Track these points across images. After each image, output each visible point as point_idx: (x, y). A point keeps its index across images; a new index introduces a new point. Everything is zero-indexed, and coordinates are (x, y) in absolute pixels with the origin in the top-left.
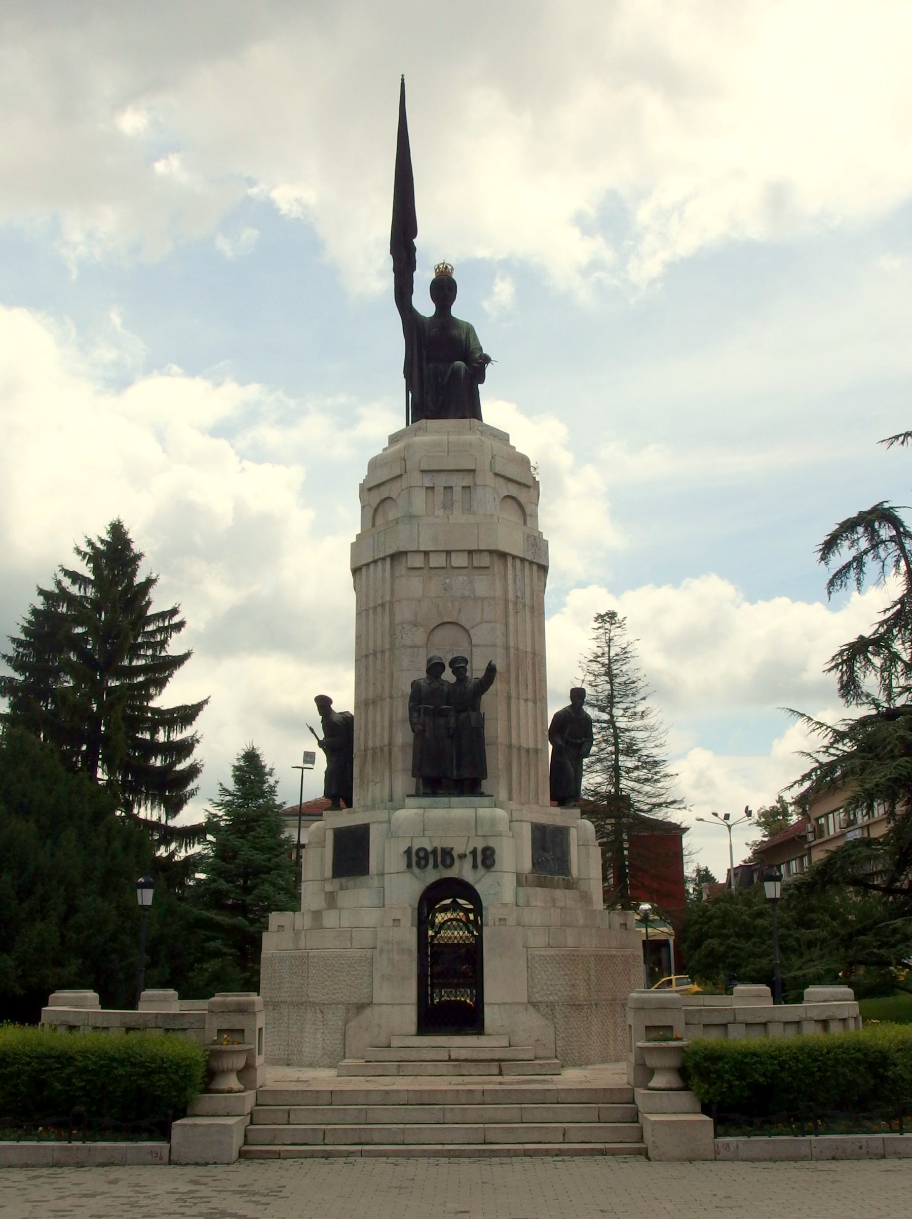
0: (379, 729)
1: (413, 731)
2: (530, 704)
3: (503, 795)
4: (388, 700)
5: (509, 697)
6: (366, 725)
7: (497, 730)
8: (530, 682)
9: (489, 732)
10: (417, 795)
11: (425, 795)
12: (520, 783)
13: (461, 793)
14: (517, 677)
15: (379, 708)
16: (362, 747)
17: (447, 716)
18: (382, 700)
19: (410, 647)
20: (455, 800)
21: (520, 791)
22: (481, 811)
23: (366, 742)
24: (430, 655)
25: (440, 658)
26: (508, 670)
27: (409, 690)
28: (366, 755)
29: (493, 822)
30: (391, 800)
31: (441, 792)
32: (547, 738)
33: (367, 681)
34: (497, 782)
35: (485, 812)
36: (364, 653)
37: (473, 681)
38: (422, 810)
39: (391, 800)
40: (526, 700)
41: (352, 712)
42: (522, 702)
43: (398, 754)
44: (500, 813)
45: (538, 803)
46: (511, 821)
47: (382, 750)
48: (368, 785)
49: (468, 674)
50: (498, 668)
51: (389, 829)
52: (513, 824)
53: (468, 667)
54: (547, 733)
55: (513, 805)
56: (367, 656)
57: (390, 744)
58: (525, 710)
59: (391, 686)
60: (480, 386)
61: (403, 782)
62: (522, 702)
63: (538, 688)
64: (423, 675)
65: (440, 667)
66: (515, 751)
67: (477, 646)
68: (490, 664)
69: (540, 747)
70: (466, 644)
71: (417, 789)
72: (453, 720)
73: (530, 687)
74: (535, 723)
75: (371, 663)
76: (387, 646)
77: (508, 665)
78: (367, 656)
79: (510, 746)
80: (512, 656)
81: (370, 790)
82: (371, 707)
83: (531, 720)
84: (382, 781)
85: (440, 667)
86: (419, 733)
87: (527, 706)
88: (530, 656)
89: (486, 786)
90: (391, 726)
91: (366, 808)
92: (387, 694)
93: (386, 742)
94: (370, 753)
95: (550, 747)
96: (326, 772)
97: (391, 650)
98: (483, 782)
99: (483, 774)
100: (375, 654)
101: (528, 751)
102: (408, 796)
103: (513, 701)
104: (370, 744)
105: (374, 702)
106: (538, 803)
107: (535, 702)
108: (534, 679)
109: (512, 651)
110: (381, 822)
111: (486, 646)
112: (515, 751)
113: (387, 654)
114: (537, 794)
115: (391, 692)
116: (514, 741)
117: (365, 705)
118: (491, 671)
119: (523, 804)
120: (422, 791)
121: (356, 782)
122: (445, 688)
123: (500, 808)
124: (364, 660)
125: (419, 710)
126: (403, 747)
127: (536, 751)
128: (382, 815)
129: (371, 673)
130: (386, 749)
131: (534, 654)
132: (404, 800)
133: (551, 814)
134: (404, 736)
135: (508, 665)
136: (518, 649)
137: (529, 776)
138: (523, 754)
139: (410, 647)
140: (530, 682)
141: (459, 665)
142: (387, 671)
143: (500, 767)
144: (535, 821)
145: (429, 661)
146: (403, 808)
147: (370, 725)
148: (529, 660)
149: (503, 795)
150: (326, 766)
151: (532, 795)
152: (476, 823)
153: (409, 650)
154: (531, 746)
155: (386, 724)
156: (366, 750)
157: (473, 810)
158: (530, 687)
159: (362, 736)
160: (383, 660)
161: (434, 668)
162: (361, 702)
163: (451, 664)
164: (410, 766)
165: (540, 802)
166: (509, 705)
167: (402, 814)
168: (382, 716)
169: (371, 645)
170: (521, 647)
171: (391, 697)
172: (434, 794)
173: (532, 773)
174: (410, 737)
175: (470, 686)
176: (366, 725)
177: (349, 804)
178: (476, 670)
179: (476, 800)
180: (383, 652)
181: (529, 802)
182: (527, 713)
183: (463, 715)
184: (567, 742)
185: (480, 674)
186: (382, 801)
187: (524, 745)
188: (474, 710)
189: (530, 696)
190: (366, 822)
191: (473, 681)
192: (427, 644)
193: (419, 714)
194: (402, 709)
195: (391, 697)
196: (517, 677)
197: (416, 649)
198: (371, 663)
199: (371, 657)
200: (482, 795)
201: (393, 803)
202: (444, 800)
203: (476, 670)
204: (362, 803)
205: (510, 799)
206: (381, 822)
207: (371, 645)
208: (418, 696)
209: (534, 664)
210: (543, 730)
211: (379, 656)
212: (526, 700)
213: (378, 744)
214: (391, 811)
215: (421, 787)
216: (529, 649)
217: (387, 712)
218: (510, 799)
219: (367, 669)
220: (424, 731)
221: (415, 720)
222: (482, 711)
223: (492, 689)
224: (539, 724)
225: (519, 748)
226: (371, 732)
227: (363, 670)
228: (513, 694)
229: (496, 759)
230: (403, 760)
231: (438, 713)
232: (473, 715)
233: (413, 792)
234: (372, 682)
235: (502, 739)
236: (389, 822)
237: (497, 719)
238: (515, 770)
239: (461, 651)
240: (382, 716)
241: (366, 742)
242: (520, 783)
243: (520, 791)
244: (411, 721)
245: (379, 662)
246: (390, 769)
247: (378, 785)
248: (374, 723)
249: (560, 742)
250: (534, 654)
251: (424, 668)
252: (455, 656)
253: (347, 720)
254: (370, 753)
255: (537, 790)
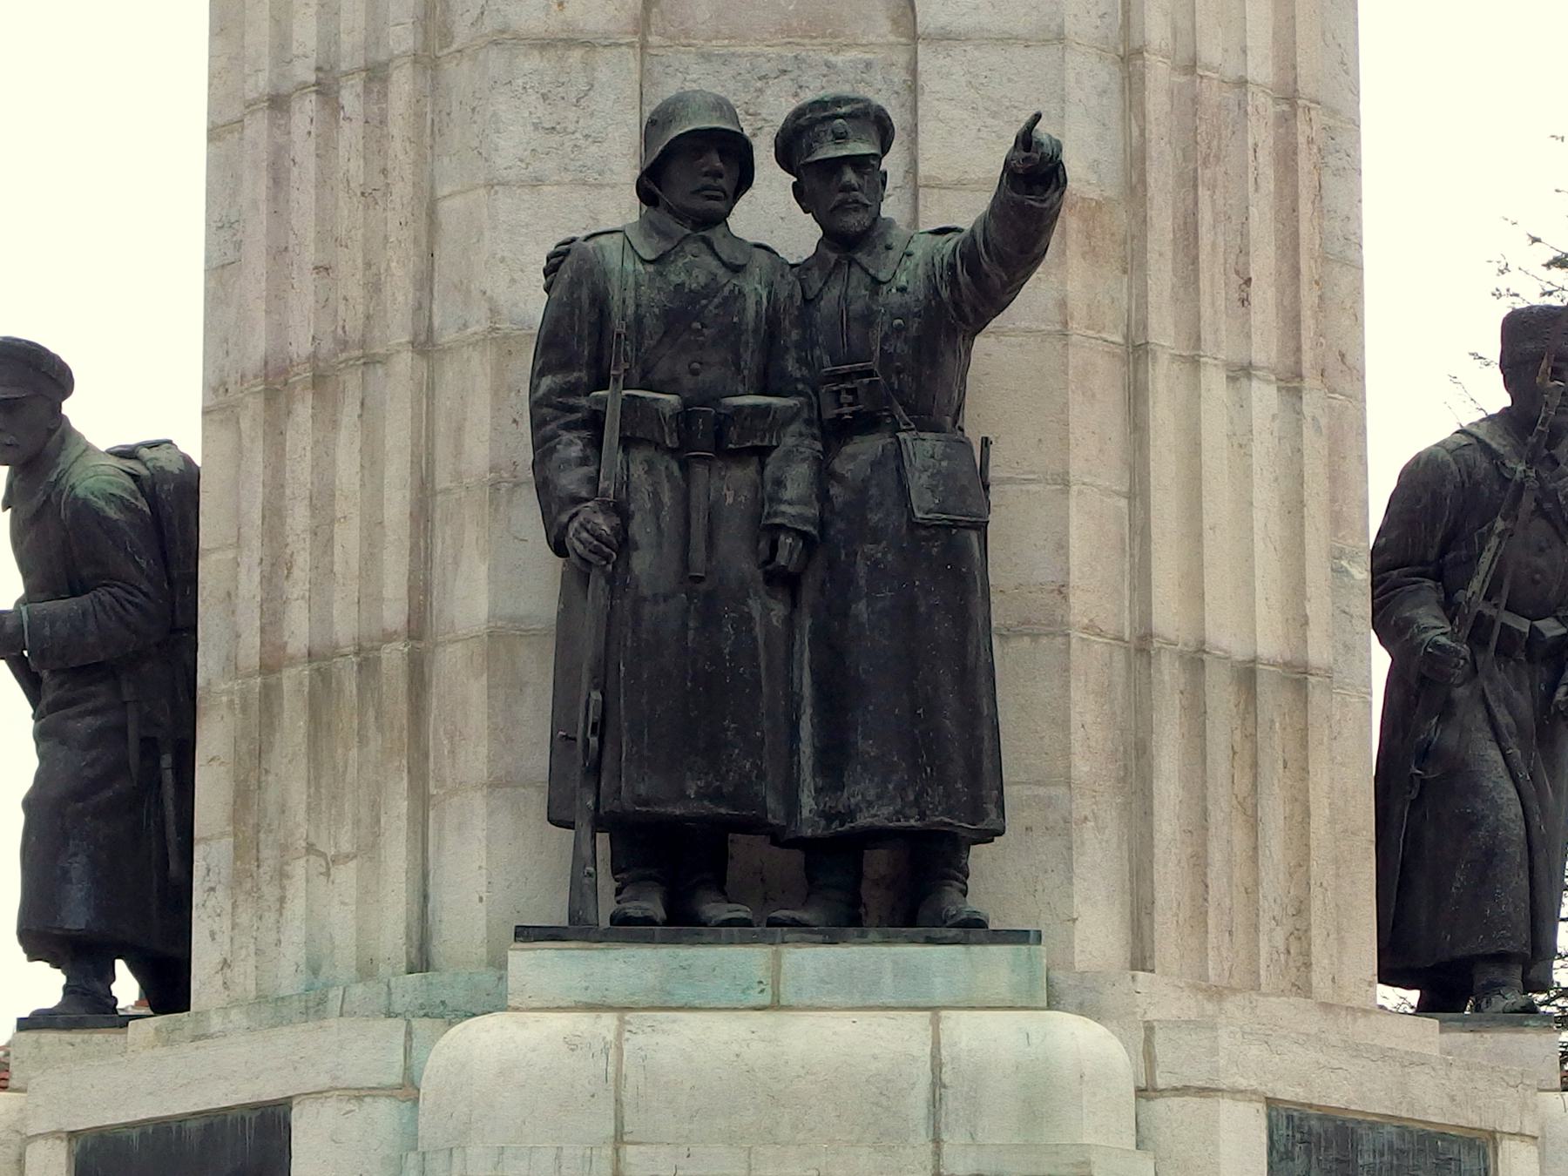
0: (348, 537)
1: (559, 548)
2: (1264, 396)
3: (1095, 933)
4: (404, 362)
5: (1137, 352)
6: (274, 514)
7: (1062, 547)
8: (1264, 263)
9: (1013, 558)
10: (577, 928)
11: (626, 928)
12: (1199, 862)
13: (846, 919)
14: (1188, 232)
15: (349, 413)
16: (251, 644)
17: (762, 453)
18: (370, 361)
19: (544, 44)
20: (808, 961)
21: (1199, 917)
22: (972, 1033)
23: (272, 620)
24: (669, 89)
25: (722, 106)
26: (1135, 190)
27: (530, 302)
28: (269, 697)
29: (1039, 1095)
30: (421, 961)
31: (716, 909)
32: (1363, 606)
33: (279, 253)
34: (1056, 860)
35: (990, 1037)
36: (261, 83)
37: (919, 249)
38: (609, 1020)
39: (421, 961)
40: (1241, 372)
41: (191, 444)
42: (1214, 381)
43: (464, 689)
44: (1078, 1038)
45: (1303, 988)
46: (1144, 1093)
47: (367, 663)
48: (282, 875)
49: (892, 208)
50: (1075, 166)
51: (410, 1139)
52: (1159, 1105)
53: (892, 163)
54: (1361, 574)
55: (1161, 996)
56: (278, 103)
57: (418, 626)
58: (1225, 428)
59: (425, 282)
60: (1509, 403)
61: (496, 851)
62: (1214, 381)
63: (1309, 297)
64: (620, 207)
65: (729, 155)
66: (1169, 673)
67: (946, 38)
68: (1026, 140)
69: (1319, 652)
70: (882, 29)
71: (581, 888)
72: (797, 480)
73: (1264, 295)
74: (1295, 509)
75: (303, 149)
76: (402, 38)
77: (1136, 161)
78: (278, 103)
79: (1142, 646)
80: (1157, 102)
81: (297, 906)
82: (303, 411)
83: (1266, 497)
84: (369, 849)
85: (729, 155)
86: (591, 557)
87: (1242, 404)
88: (1263, 105)
89: (993, 877)
90: (422, 515)
91: (270, 1008)
92: (397, 332)
93: (394, 614)
94: (294, 680)
95: (1380, 661)
96: (29, 804)
97: (427, 62)
98: (980, 857)
99: (982, 816)
100: (326, 89)
101: (1247, 675)
102: (525, 934)
103: (1163, 378)
104: (298, 631)
105: (321, 381)
106: (1303, 988)
107: (1291, 384)
108: (1290, 246)
109: (1159, 74)
110: (359, 1094)
111: (1006, 40)
112: (1169, 673)
113: (402, 84)
114: (1301, 935)
115: (422, 308)
116: (1168, 617)
117: (271, 395)
118: (1034, 175)
119: (1216, 993)
120: (607, 905)
121: (211, 858)
122: (754, 288)
123: (1082, 1010)
124: (258, 126)
125: (595, 423)
126: (500, 639)
127: (1298, 676)
128: (368, 1049)
129: (303, 199)
130: (394, 656)
131: (1289, 96)
132: (498, 964)
133: (1385, 1055)
134: (500, 578)
135: (1136, 161)
136: (1191, 66)
137: (1254, 824)
138: (1221, 696)
139: (544, 44)
140: (1264, 263)
141: (837, 154)
142: (402, 191)
143: (1082, 767)
144: (1289, 1092)
145: (653, 126)
146: (497, 1003)
147: (299, 518)
148: (1261, 133)
149: (1095, 933)
150: (33, 763)
151: (1272, 938)
152: (937, 1084)
153: (531, 62)
154: (1269, 644)
155: (397, 505)
156: (271, 665)
157: (918, 1022)
158: (1264, 295)
159: (250, 585)
160: (376, 124)
161: (690, 168)
162: (259, 385)
163: (789, 149)
164: (539, 762)
165: (1319, 979)
166: (1136, 397)
167: (484, 1040)
168: (372, 461)
169: (306, 34)
170: (1211, 52)
171: (425, 345)
172: (681, 920)
173: (1274, 812)
174: (537, 584)
175: (907, 271)
176: (274, 514)
177: (169, 989)
178: (943, 182)
179: (938, 962)
180: (376, 75)
181: (1256, 987)
182: (1241, 445)
183: (863, 451)
184: (1478, 631)
185: (967, 208)
186: (366, 970)
187: (1224, 636)
188: (926, 421)
189: (1265, 349)
190: (268, 1091)
191: (919, 249)
192: (643, 25)
193: (596, 443)
194: (488, 417)
195: (425, 345)
196: (1188, 232)
197: (576, 55)
198: (303, 149)
199: (306, 109)
200: (973, 929)
201: (429, 978)
202: (745, 960)
203: (943, 182)
204: (245, 977)
205: (1141, 960)
206: (359, 1094)
207: (306, 34)
208: (584, 343)
209: (1286, 159)
210: (1336, 555)
211: (350, 98)
212: (1241, 372)
213: (345, 627)
214: (421, 1026)
215: (606, 883)
216: (1261, 69)
217: (397, 435)
218: (1141, 960)
219: (278, 180)
220: (623, 543)
221: (571, 481)
222: (973, 434)
223: (1037, 295)
224: (1316, 510)
225: (1196, 659)
226: (302, 561)
227: (256, 186)
228: (1163, 332)
229: (1055, 716)
230: (494, 726)
231: (708, 437)
232: (923, 448)
233: (558, 916)
234: (310, 256)
235: (1092, 599)
236: (408, 1090)
237: (1063, 482)
238: (1168, 791)
239: (854, 68)
240: (372, 461)
241: (272, 620)
242: (1199, 862)
243: (1199, 917)
244: (544, 488)
245: (350, 135)
246: (422, 802)
247: (346, 875)
248: (322, 501)
249: (1431, 624)
250: (1289, 96)
251: (627, 170)
252: (809, 96)
253: (164, 502)
254: (294, 680)
255: (1301, 909)
